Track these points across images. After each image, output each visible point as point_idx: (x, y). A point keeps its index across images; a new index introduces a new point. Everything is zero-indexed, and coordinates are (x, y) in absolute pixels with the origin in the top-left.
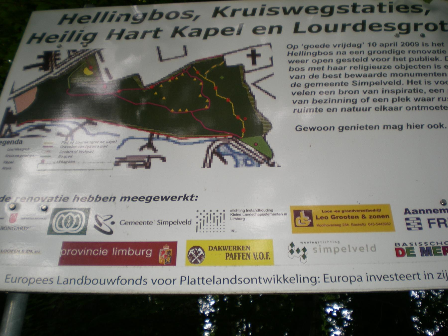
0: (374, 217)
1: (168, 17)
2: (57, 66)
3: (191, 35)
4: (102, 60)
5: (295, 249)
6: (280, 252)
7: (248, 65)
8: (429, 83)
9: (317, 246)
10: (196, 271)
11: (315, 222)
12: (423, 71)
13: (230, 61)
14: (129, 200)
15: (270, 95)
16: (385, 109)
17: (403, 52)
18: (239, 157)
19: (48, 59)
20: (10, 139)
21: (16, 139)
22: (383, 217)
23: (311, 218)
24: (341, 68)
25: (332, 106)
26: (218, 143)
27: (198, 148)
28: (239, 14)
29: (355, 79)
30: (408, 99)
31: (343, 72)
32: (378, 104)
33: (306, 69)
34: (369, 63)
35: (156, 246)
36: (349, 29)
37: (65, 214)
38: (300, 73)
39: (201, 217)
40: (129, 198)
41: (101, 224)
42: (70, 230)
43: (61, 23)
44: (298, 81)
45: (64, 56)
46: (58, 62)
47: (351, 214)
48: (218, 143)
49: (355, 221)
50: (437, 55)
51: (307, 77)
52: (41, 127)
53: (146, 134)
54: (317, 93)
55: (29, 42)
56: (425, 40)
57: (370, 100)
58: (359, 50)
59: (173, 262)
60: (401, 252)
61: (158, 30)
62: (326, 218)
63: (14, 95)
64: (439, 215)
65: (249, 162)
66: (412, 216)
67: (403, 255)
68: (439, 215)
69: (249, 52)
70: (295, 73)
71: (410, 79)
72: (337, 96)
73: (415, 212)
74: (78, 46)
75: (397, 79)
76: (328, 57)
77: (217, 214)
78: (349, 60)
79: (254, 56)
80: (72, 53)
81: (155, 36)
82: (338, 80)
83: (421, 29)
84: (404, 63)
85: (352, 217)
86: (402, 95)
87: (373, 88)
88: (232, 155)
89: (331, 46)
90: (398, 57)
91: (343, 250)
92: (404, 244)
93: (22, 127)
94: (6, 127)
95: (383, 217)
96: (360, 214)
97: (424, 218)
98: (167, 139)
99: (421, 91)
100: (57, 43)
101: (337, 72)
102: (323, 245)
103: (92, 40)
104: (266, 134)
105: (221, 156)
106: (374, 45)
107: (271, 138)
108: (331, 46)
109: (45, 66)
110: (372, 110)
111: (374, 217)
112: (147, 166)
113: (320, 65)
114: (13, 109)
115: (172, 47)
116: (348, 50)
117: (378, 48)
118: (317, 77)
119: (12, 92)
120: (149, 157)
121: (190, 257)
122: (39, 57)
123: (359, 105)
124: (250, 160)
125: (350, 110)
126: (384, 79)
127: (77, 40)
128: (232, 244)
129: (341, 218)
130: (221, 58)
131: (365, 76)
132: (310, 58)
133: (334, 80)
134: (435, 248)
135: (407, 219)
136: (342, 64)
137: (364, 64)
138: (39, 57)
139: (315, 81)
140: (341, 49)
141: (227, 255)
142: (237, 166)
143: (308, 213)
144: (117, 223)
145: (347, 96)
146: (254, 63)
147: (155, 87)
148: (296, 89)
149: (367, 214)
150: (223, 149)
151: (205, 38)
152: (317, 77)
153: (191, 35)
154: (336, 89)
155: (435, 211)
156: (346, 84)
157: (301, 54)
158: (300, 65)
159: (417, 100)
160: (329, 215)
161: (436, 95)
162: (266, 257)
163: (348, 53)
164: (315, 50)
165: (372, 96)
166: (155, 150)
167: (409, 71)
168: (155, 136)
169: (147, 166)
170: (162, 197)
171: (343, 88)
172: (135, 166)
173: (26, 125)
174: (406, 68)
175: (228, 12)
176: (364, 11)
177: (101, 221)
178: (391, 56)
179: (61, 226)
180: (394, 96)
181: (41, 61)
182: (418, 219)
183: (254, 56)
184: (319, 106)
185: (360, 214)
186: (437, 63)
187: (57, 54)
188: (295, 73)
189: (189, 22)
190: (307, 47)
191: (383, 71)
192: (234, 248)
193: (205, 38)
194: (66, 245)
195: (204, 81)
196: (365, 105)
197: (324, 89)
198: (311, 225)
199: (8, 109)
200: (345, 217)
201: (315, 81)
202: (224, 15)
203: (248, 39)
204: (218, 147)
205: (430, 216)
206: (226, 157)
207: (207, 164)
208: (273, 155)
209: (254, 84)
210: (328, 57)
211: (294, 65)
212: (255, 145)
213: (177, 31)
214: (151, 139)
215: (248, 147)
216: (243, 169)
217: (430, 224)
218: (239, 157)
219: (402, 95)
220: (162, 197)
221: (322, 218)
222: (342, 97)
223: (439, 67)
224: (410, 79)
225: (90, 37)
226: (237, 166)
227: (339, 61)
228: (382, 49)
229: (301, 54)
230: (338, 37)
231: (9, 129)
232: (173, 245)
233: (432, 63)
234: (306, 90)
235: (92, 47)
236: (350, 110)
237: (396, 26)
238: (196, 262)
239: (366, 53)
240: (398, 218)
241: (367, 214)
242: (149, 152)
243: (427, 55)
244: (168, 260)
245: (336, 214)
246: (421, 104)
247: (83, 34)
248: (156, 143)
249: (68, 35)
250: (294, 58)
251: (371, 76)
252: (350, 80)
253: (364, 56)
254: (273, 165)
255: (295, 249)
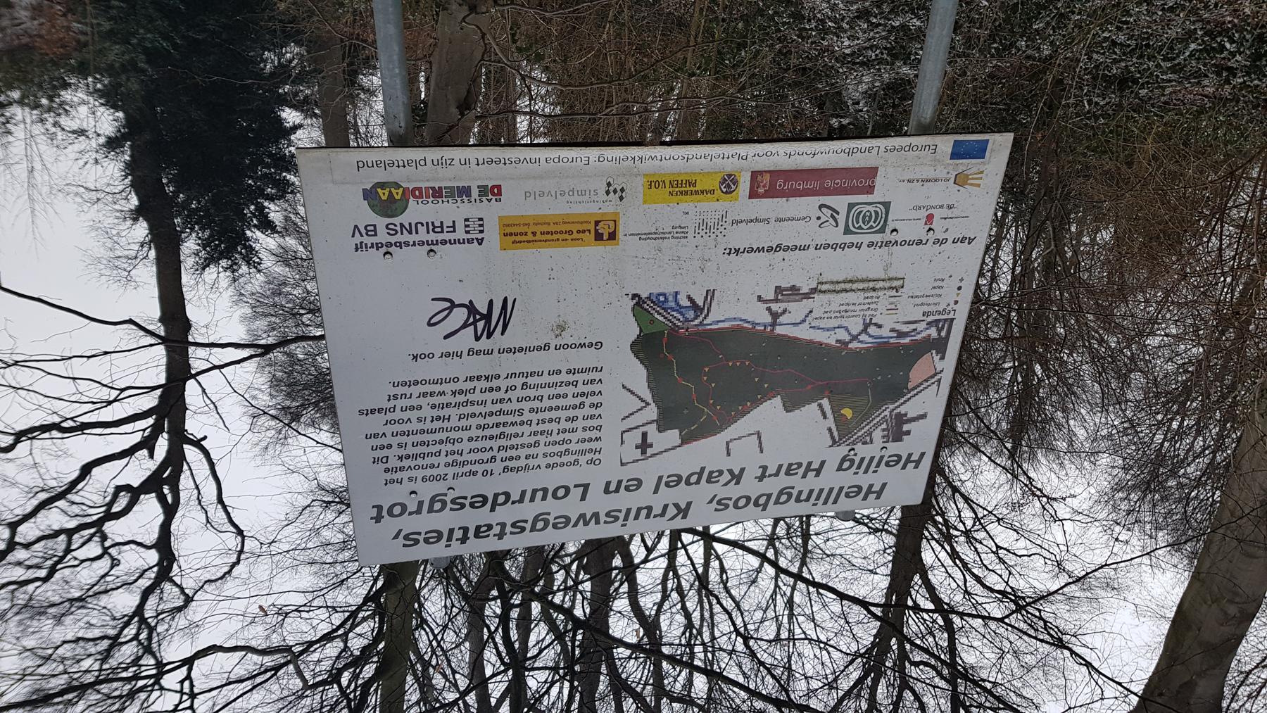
0: (521, 234)
1: (748, 499)
2: (884, 420)
3: (721, 473)
4: (830, 430)
5: (619, 193)
6: (636, 187)
7: (652, 430)
8: (419, 420)
9: (594, 198)
10: (729, 165)
11: (592, 227)
12: (425, 437)
13: (673, 436)
14: (544, 498)
15: (629, 390)
16: (487, 378)
17: (447, 465)
18: (673, 304)
19: (897, 431)
20: (937, 317)
21: (931, 318)
22: (511, 234)
23: (596, 231)
24: (535, 433)
25: (555, 379)
26: (696, 322)
27: (720, 315)
28: (657, 510)
29: (518, 419)
30: (454, 393)
31: (534, 428)
32: (495, 383)
33: (580, 430)
34: (495, 444)
35: (771, 193)
36: (515, 496)
37: (871, 227)
38: (589, 423)
39: (721, 229)
40: (545, 490)
41: (832, 216)
42: (866, 208)
43: (884, 485)
44: (593, 411)
45: (878, 435)
46: (884, 426)
47: (549, 237)
48: (696, 322)
49: (545, 228)
50: (399, 464)
51: (580, 418)
52: (901, 334)
53: (779, 330)
54: (570, 396)
55: (923, 454)
56: (412, 486)
57: (503, 389)
58: (507, 463)
59: (755, 175)
60: (494, 192)
61: (761, 479)
62: (578, 232)
63: (936, 378)
64: (440, 237)
65: (662, 299)
66: (474, 236)
67: (493, 187)
68: (440, 237)
69: (649, 451)
70: (595, 422)
71: (446, 424)
72: (546, 392)
73: (470, 241)
74: (863, 451)
75: (464, 423)
76: (551, 449)
77: (702, 233)
78: (523, 446)
79: (644, 445)
80: (868, 439)
81: (765, 468)
82: (541, 416)
83: (412, 507)
84: (450, 447)
85: (548, 233)
86: (461, 398)
87: (498, 407)
88: (681, 307)
89: (543, 466)
90: (456, 456)
91: (563, 194)
92: (489, 201)
93: (924, 334)
94: (943, 334)
95: (511, 234)
96: (539, 237)
97: (460, 234)
98: (754, 324)
99: (433, 407)
100: (886, 453)
101: (541, 427)
102: (586, 198)
103: (844, 460)
104: (639, 336)
105: (694, 305)
106: (485, 473)
107: (634, 331)
108: (543, 466)
109: (901, 419)
110: (503, 376)
111: (521, 234)
112: (778, 289)
113: (561, 436)
114: (937, 358)
115: (746, 456)
116: (522, 462)
117: (479, 468)
118: (568, 419)
119: (939, 381)
120: (776, 301)
121: (736, 182)
122: (908, 433)
123: (518, 382)
124: (658, 300)
125: (532, 374)
126: (481, 421)
127: (863, 459)
128: (684, 178)
129: (561, 232)
130: (685, 441)
131: (504, 425)
132: (573, 447)
133: (547, 415)
134: (452, 196)
135: (482, 232)
136: (532, 440)
137: (503, 442)
138: (908, 433)
139: (571, 413)
140: (531, 462)
141: (694, 185)
142: (677, 293)
143: (599, 237)
144: (814, 218)
145: (532, 393)
146: (644, 435)
147: (767, 396)
148: (595, 400)
149: (530, 237)
150: (691, 314)
151: (703, 469)
152: (568, 419)
153: (721, 473)
154: (546, 403)
155: (444, 242)
156: (531, 411)
157: (583, 453)
158: (587, 435)
159: (442, 393)
160: (575, 235)
161: (414, 402)
162: (654, 184)
163: (523, 457)
164: (565, 459)
165: (501, 395)
166: (769, 309)
167: (443, 436)
168: (769, 329)
169: (778, 289)
170: (597, 522)
171: (536, 404)
172: (793, 288)
173: (919, 337)
174: (448, 440)
175: (672, 511)
176: (490, 527)
177: (831, 220)
178: (466, 457)
179: (876, 212)
180: (471, 397)
181: (906, 427)
182: (468, 232)
183: (644, 445)
184: (571, 378)
185: (539, 237)
186: (402, 452)
187: (886, 438)
188: (595, 422)
189: (722, 492)
190: (576, 462)
191: (480, 433)
192: (686, 193)
193: (703, 469)
194: (870, 190)
195: (707, 406)
196: (510, 382)
197: (561, 402)
198: (597, 223)
199: (942, 358)
200: (556, 233)
201: (571, 413)
202: (676, 506)
203: (649, 471)
204: (696, 317)
205: (452, 236)
206: (688, 304)
207: (710, 295)
208: (633, 309)
209: (648, 404)
210: (551, 449)
211: (594, 434)
212: (653, 321)
213: (737, 478)
214: (774, 324)
215: (661, 319)
216: (669, 290)
217: (454, 226)
218: (673, 304)
219: (461, 398)
220: (597, 522)
221: (584, 232)
222: (541, 392)
223: (400, 446)
224: (446, 424)
225: (846, 464)
226: (677, 293)
227: (537, 443)
228: (474, 468)
229: (583, 453)
230: (529, 481)
231: (939, 331)
232: (753, 195)
233: (411, 450)
234: (584, 399)
235: (843, 450)
236: (532, 374)
237: (449, 505)
238: (729, 176)
239: (498, 459)
240: (492, 234)
241: (530, 237)
242: (775, 307)
243: (412, 464)
244: (759, 178)
245: (567, 236)
246: (437, 388)
247: (854, 469)
248: (768, 319)
249: (872, 468)
250: (593, 445)
251: (497, 425)
252: (527, 416)
253: (503, 454)
254: (635, 296)
255: (619, 193)
